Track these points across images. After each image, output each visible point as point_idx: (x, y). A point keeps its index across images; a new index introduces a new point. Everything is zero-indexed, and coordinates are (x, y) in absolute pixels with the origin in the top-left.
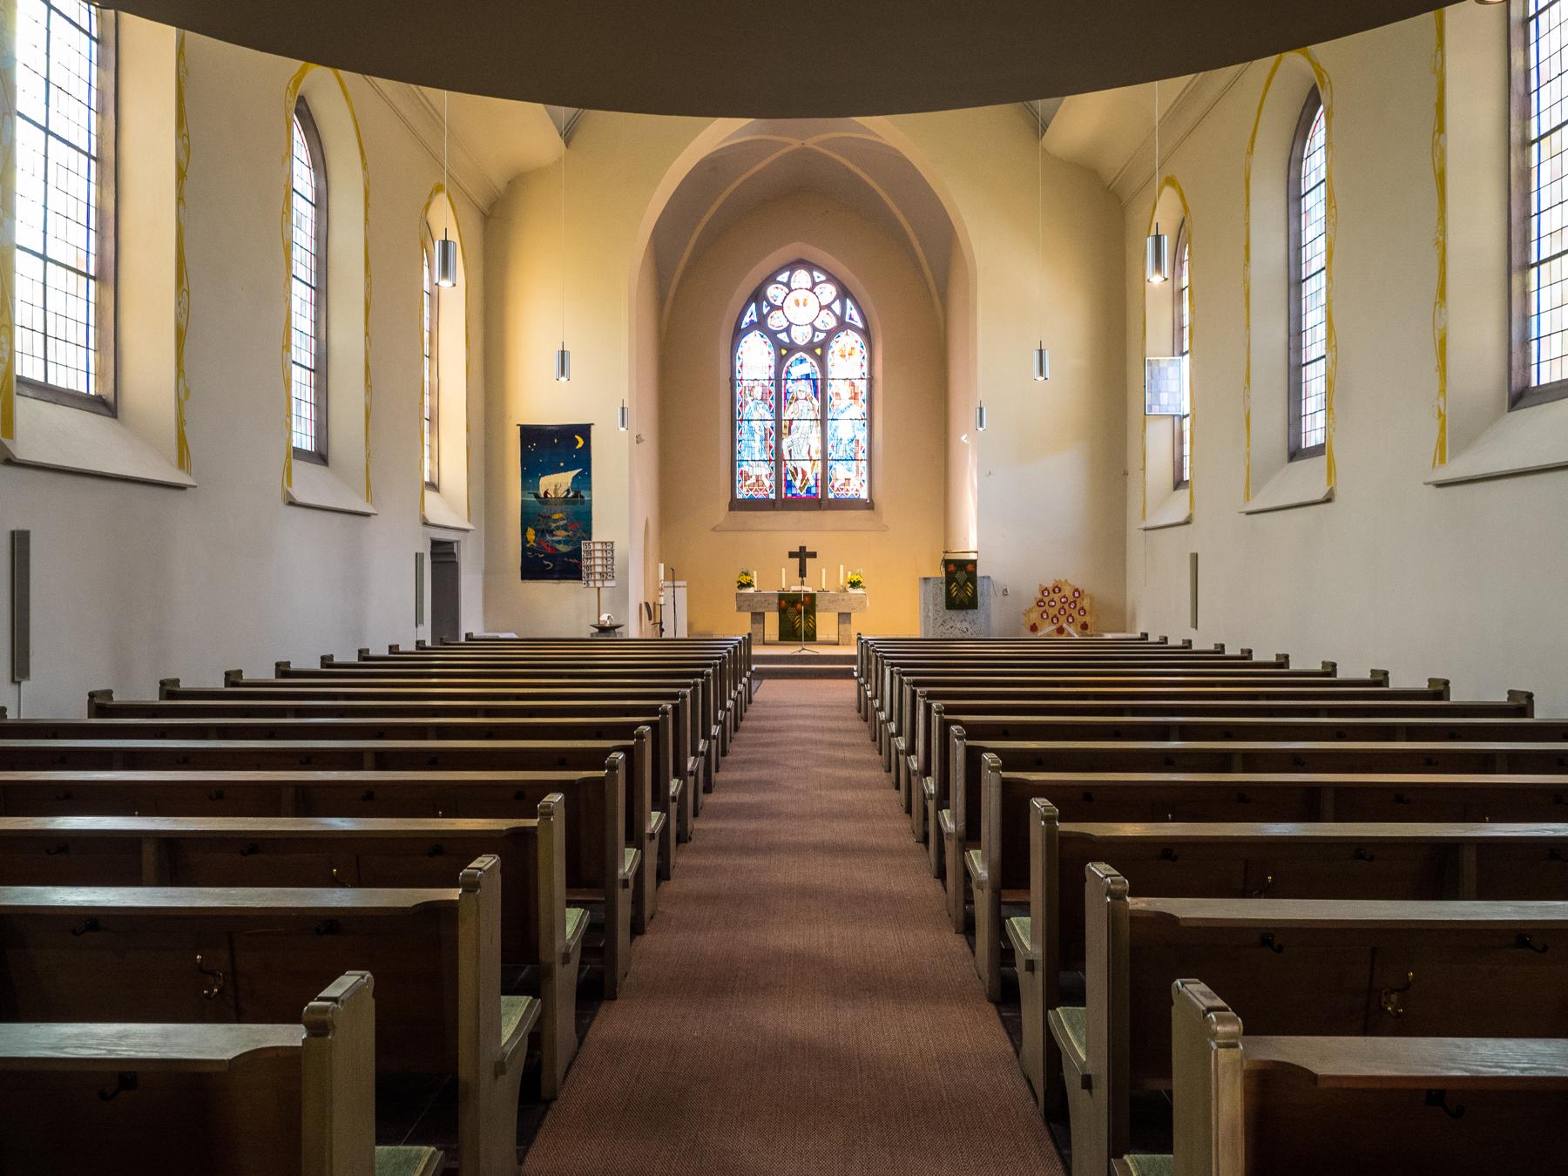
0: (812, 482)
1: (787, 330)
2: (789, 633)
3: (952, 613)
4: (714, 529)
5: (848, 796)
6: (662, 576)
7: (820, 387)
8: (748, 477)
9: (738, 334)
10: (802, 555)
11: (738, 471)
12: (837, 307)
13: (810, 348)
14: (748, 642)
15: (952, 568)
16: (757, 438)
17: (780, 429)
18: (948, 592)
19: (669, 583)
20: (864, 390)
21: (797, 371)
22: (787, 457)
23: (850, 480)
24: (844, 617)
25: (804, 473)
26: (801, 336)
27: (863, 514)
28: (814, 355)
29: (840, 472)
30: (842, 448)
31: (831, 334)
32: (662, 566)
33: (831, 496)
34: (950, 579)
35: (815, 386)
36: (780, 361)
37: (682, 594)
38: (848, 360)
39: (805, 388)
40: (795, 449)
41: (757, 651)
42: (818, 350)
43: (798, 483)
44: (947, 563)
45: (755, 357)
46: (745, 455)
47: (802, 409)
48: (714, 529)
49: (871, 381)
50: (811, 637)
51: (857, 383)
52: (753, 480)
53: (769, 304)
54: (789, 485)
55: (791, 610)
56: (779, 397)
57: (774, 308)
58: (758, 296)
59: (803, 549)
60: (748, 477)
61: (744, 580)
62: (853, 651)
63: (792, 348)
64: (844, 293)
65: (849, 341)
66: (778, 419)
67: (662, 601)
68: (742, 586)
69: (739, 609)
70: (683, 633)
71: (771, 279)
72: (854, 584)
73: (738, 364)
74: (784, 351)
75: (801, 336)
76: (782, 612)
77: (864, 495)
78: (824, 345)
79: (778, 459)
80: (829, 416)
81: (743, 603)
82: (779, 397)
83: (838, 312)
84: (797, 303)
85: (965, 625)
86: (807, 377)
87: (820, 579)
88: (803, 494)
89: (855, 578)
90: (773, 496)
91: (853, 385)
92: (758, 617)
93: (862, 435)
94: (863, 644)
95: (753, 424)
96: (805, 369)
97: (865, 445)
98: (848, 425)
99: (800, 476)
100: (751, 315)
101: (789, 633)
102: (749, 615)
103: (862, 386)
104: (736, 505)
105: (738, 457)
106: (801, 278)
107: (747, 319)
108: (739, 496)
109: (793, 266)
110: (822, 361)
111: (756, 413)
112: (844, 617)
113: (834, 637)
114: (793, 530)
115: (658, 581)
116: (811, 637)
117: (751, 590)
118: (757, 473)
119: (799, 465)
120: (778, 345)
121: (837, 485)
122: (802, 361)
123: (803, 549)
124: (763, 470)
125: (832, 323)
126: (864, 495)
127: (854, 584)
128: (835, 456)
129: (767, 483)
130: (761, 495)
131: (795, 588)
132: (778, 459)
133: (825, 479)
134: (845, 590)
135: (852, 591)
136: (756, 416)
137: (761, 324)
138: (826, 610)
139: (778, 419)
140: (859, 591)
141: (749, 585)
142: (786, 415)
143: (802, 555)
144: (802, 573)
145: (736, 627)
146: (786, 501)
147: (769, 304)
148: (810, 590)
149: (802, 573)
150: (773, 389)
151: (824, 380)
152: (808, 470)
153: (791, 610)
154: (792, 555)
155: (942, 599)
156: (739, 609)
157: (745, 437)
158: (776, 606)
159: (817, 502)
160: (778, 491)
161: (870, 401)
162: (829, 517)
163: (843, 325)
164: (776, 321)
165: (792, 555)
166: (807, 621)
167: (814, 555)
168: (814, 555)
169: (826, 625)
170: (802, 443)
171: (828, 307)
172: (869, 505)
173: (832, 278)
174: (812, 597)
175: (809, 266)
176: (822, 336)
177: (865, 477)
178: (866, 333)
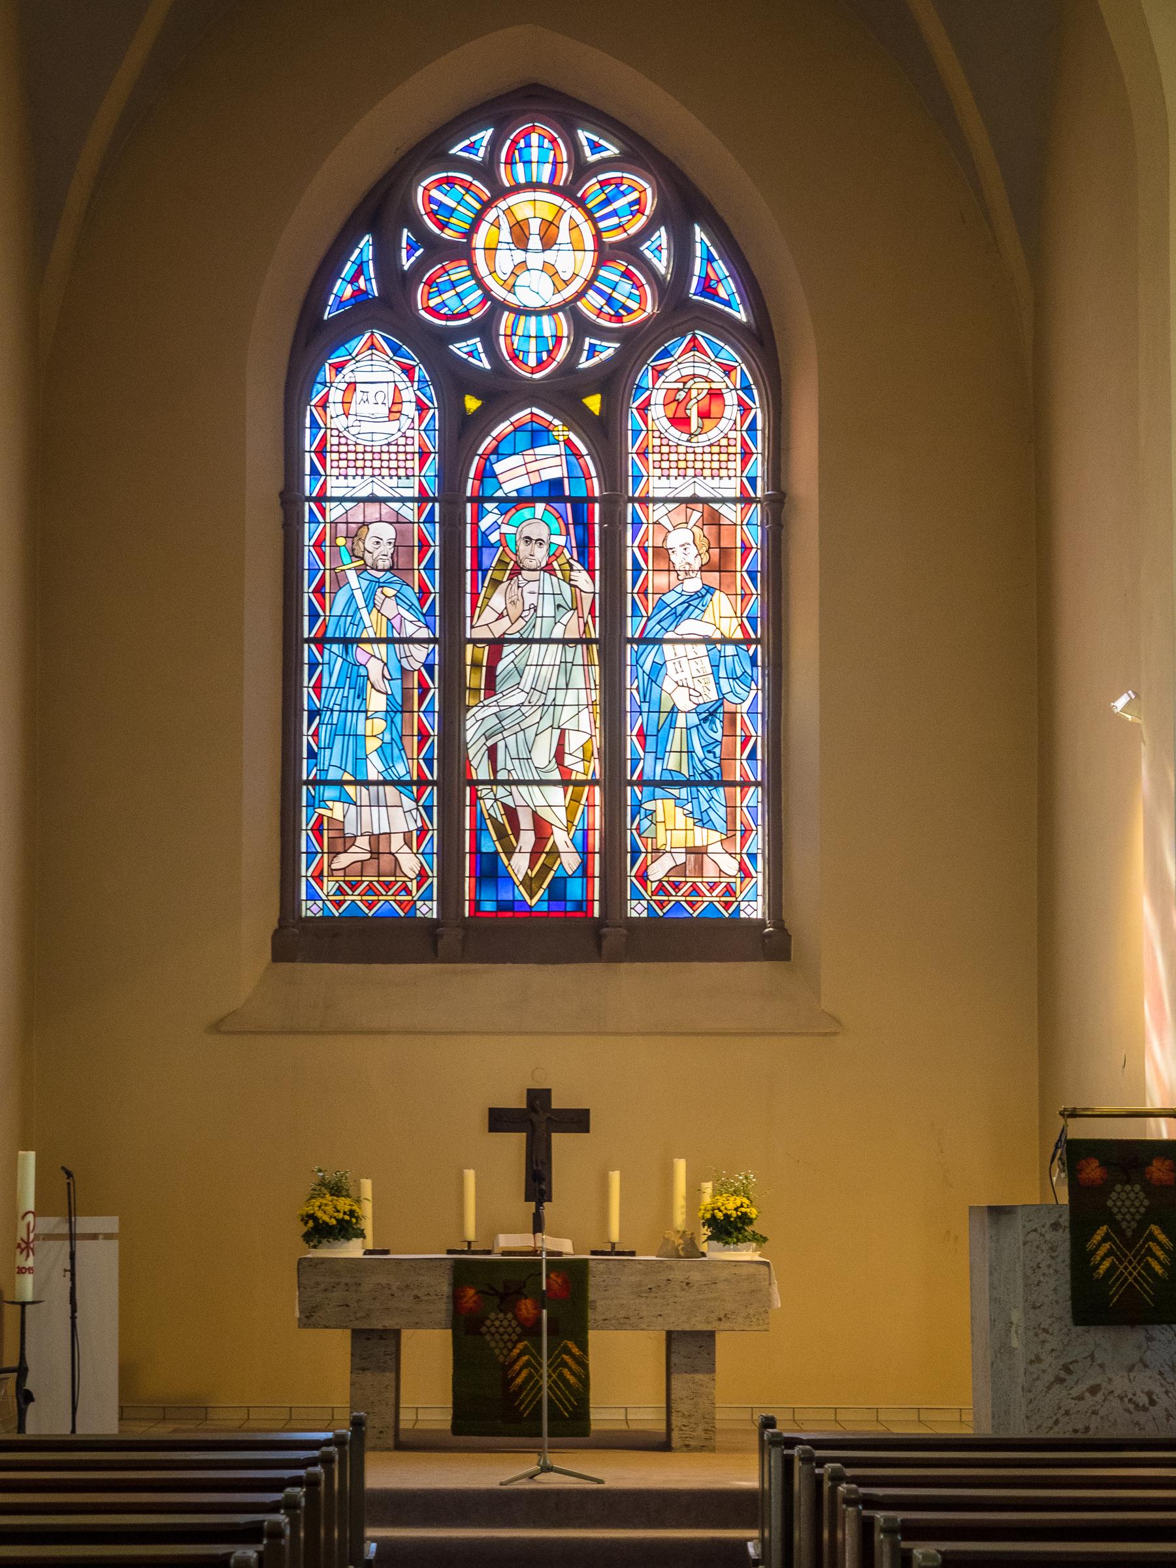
0: (570, 862)
1: (485, 328)
2: (490, 1408)
3: (1097, 1338)
4: (217, 1027)
5: (184, 1427)
6: (29, 1202)
7: (599, 526)
8: (344, 842)
9: (315, 339)
10: (537, 1122)
11: (306, 820)
12: (659, 252)
13: (563, 391)
14: (353, 1446)
15: (1093, 1170)
16: (377, 702)
17: (456, 672)
18: (1080, 1260)
19: (54, 1224)
20: (755, 536)
21: (513, 473)
22: (482, 771)
23: (699, 848)
24: (689, 1349)
25: (541, 828)
26: (532, 343)
27: (752, 973)
28: (577, 418)
29: (671, 829)
30: (676, 740)
31: (640, 344)
32: (29, 1159)
33: (637, 910)
34: (1086, 1210)
35: (582, 522)
36: (459, 440)
37: (101, 1262)
38: (699, 449)
39: (542, 528)
40: (509, 745)
41: (384, 1474)
42: (593, 398)
43: (519, 865)
44: (1075, 1153)
45: (370, 404)
46: (333, 763)
47: (536, 601)
48: (217, 1027)
49: (777, 507)
50: (571, 1422)
51: (730, 513)
52: (359, 851)
53: (423, 237)
54: (490, 871)
55: (497, 1321)
56: (453, 562)
57: (440, 251)
58: (382, 209)
59: (538, 1098)
60: (344, 842)
61: (329, 1210)
62: (743, 1474)
63: (502, 390)
64: (683, 205)
65: (700, 366)
66: (450, 636)
67: (27, 1287)
68: (319, 1232)
69: (310, 1318)
70: (102, 1418)
71: (430, 151)
72: (727, 1229)
73: (309, 443)
74: (470, 399)
75: (532, 343)
76: (466, 1328)
77: (754, 909)
78: (615, 380)
79: (448, 781)
80: (632, 628)
81: (324, 1295)
82: (453, 562)
83: (662, 264)
84: (520, 236)
85: (1143, 1383)
86: (552, 492)
87: (606, 1206)
88: (537, 901)
89: (731, 1204)
90: (429, 910)
91: (714, 520)
92: (376, 1349)
93: (748, 700)
94: (773, 1440)
95: (361, 653)
96: (549, 463)
97: (757, 730)
98: (691, 671)
99: (527, 840)
100: (357, 275)
101: (490, 1408)
102: (348, 1332)
103: (747, 528)
104: (303, 940)
105: (306, 771)
106: (539, 152)
107: (343, 289)
108: (310, 909)
109: (508, 107)
110: (605, 436)
111: (376, 620)
112: (689, 1349)
113: (647, 1416)
114: (503, 1032)
115: (13, 1212)
116: (571, 1422)
117: (353, 1250)
118: (376, 823)
119: (522, 797)
120: (451, 379)
121: (658, 870)
122: (538, 436)
123: (538, 1098)
124: (396, 817)
125: (643, 307)
126: (754, 909)
127: (727, 1229)
128: (650, 768)
129: (410, 864)
130: (389, 903)
131: (513, 1242)
132: (448, 781)
133: (615, 850)
134: (692, 1250)
135: (718, 1253)
136: (372, 625)
137: (390, 311)
138: (624, 1323)
139: (450, 636)
140: (747, 1253)
141: (346, 1229)
142: (485, 622)
143: (537, 1122)
144: (538, 1185)
145: (301, 1384)
146: (487, 921)
147: (423, 237)
148: (566, 1247)
149: (538, 1185)
150: (434, 535)
151: (614, 502)
152: (557, 816)
153: (497, 1321)
154: (499, 1120)
155: (1057, 1287)
156: (310, 1318)
157: (333, 698)
158: (442, 1308)
159: (592, 930)
160: (449, 893)
161: (775, 577)
162: (632, 985)
163: (680, 312)
164: (448, 297)
165: (499, 1120)
166: (557, 1365)
167: (578, 1121)
168: (578, 1121)
169: (624, 1374)
170: (539, 724)
171: (630, 249)
172: (771, 943)
173: (640, 152)
174: (573, 1274)
175: (564, 109)
176: (608, 350)
177: (757, 842)
178: (762, 344)
